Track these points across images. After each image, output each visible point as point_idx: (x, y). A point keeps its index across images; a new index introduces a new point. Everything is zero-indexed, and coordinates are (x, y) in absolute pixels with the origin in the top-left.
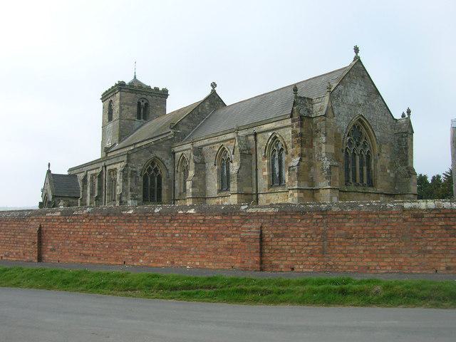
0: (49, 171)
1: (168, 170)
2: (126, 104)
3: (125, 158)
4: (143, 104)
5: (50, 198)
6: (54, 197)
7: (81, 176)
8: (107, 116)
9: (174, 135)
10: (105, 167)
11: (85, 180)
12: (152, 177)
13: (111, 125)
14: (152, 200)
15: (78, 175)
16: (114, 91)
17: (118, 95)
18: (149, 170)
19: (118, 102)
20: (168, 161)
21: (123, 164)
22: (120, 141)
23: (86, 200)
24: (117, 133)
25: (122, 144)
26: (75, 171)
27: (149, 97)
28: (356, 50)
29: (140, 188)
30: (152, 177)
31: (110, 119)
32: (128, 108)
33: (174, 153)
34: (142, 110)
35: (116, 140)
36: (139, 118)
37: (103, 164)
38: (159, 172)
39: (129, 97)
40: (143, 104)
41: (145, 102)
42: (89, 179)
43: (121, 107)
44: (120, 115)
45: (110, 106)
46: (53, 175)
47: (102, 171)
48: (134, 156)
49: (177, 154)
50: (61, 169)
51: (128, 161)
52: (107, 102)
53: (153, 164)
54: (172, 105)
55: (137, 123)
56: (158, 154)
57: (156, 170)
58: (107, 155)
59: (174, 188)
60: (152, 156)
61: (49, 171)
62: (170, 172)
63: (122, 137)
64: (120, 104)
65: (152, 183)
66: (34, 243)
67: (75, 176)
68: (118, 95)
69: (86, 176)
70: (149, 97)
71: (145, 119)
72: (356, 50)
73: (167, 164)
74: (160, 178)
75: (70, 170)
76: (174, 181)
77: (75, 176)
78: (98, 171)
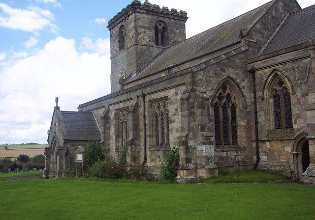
0: (57, 108)
1: (244, 97)
2: (143, 27)
3: (188, 79)
4: (160, 27)
5: (61, 143)
6: (66, 141)
7: (101, 112)
8: (117, 44)
10: (144, 96)
11: (106, 118)
12: (225, 108)
13: (124, 53)
14: (227, 143)
16: (127, 13)
17: (132, 17)
18: (220, 97)
19: (132, 25)
20: (245, 84)
22: (138, 71)
23: (109, 144)
25: (143, 73)
26: (89, 108)
27: (167, 20)
28: (57, 100)
29: (211, 125)
30: (225, 108)
31: (122, 46)
33: (253, 71)
34: (160, 36)
35: (133, 69)
36: (157, 44)
37: (139, 92)
38: (233, 100)
39: (144, 19)
40: (160, 27)
41: (163, 25)
43: (137, 31)
44: (137, 40)
45: (121, 33)
46: (63, 113)
47: (137, 103)
48: (201, 76)
49: (258, 73)
50: (70, 105)
51: (194, 83)
52: (117, 29)
53: (224, 88)
54: (192, 29)
55: (156, 50)
56: (231, 72)
57: (229, 97)
58: (122, 88)
59: (257, 123)
60: (224, 75)
61: (57, 108)
62: (247, 100)
63: (139, 67)
64: (136, 28)
65: (225, 118)
66: (212, 121)
67: (89, 113)
69: (108, 111)
70: (167, 20)
71: (163, 44)
72: (57, 100)
73: (244, 87)
74: (233, 108)
75: (81, 106)
76: (256, 113)
77: (89, 113)
78: (134, 102)
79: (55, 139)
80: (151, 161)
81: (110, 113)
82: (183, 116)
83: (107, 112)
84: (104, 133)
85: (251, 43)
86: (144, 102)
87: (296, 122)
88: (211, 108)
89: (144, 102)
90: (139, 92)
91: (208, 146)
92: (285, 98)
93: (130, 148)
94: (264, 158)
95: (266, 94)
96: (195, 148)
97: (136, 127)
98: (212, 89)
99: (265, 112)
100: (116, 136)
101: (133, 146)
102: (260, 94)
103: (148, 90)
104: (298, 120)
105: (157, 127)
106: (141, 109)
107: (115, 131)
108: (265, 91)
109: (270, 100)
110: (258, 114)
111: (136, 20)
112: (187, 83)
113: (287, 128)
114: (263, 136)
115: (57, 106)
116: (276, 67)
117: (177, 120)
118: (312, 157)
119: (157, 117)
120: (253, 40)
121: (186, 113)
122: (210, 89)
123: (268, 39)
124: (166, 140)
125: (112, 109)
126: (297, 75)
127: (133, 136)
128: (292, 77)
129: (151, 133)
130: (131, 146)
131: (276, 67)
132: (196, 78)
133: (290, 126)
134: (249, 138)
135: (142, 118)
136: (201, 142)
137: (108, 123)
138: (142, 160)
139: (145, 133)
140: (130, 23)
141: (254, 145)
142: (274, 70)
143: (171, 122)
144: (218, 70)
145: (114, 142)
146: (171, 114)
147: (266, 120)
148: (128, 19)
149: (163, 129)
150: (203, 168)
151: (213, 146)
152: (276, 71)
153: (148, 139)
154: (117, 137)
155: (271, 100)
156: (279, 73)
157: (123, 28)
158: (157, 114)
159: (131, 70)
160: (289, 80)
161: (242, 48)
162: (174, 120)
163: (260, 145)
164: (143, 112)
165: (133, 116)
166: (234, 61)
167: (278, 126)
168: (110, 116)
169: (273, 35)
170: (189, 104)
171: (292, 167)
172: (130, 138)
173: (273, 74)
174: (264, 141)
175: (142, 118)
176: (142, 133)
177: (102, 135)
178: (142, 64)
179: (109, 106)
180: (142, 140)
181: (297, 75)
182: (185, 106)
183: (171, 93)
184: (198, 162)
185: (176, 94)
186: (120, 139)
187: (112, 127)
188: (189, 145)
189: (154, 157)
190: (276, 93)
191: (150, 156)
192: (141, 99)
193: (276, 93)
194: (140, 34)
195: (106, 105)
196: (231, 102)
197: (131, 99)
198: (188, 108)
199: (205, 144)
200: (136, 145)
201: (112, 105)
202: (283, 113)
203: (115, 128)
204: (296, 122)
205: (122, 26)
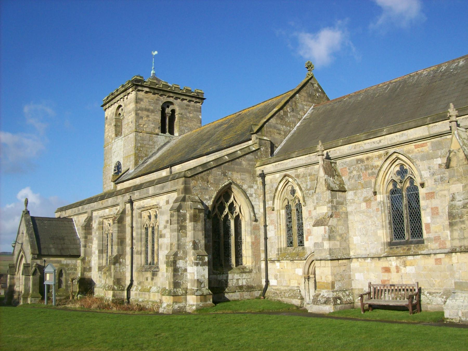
9: (260, 145)
10: (131, 202)
11: (88, 227)
15: (75, 218)
17: (132, 95)
19: (132, 106)
21: (174, 196)
23: (90, 261)
24: (133, 152)
32: (148, 116)
36: (163, 131)
37: (127, 197)
38: (237, 210)
42: (95, 225)
43: (137, 114)
46: (33, 218)
47: (124, 212)
49: (268, 178)
68: (132, 95)
73: (251, 195)
79: (21, 253)
80: (138, 284)
81: (93, 222)
82: (172, 231)
83: (90, 220)
84: (85, 246)
85: (263, 142)
86: (132, 209)
87: (307, 240)
88: (189, 225)
89: (132, 209)
90: (127, 197)
91: (200, 268)
92: (297, 210)
93: (113, 267)
94: (273, 282)
95: (278, 204)
96: (186, 270)
97: (121, 241)
98: (210, 198)
99: (275, 226)
100: (99, 250)
101: (117, 265)
102: (269, 204)
103: (136, 194)
104: (309, 237)
105: (147, 241)
106: (128, 220)
107: (99, 245)
108: (276, 200)
109: (281, 211)
110: (268, 228)
111: (138, 100)
112: (179, 190)
113: (299, 246)
114: (272, 254)
115: (26, 210)
116: (288, 173)
117: (168, 235)
118: (319, 282)
119: (147, 229)
120: (265, 138)
121: (175, 226)
122: (207, 197)
123: (285, 135)
124: (156, 258)
125: (96, 217)
126: (309, 183)
127: (118, 252)
128: (303, 186)
129: (139, 249)
130: (114, 264)
131: (288, 173)
132: (190, 184)
133: (301, 243)
134: (256, 256)
135: (128, 230)
136: (193, 262)
137: (91, 234)
138: (128, 283)
139: (132, 248)
140: (129, 104)
141: (263, 265)
142: (285, 176)
143: (161, 237)
144: (219, 175)
145: (97, 258)
146: (161, 227)
147: (277, 235)
148: (127, 98)
149: (153, 245)
150: (193, 294)
151: (206, 268)
152: (287, 177)
153: (135, 256)
154: (101, 252)
155: (283, 212)
156: (290, 180)
157: (121, 108)
158: (147, 225)
159: (128, 164)
160: (301, 189)
161: (251, 147)
162: (164, 235)
163: (270, 265)
164: (130, 222)
165: (119, 227)
166: (241, 164)
167: (290, 244)
168: (93, 226)
169: (292, 132)
170: (179, 216)
171: (303, 293)
172: (115, 254)
173: (284, 181)
174: (273, 261)
175: (128, 230)
176: (128, 249)
177: (82, 249)
178: (142, 157)
179: (92, 212)
180: (128, 257)
181: (309, 183)
182: (175, 218)
183: (161, 200)
184: (189, 287)
185: (168, 202)
186: (105, 255)
187: (95, 239)
188: (178, 266)
189: (141, 279)
190: (288, 203)
191: (137, 278)
192: (128, 205)
193: (288, 203)
194: (142, 118)
195: (89, 211)
196: (236, 213)
197: (118, 205)
198: (178, 220)
199: (197, 264)
200: (120, 263)
201: (95, 210)
202: (295, 228)
203: (99, 241)
204: (307, 240)
205: (120, 106)
